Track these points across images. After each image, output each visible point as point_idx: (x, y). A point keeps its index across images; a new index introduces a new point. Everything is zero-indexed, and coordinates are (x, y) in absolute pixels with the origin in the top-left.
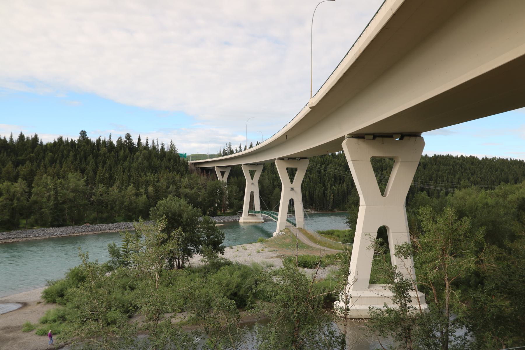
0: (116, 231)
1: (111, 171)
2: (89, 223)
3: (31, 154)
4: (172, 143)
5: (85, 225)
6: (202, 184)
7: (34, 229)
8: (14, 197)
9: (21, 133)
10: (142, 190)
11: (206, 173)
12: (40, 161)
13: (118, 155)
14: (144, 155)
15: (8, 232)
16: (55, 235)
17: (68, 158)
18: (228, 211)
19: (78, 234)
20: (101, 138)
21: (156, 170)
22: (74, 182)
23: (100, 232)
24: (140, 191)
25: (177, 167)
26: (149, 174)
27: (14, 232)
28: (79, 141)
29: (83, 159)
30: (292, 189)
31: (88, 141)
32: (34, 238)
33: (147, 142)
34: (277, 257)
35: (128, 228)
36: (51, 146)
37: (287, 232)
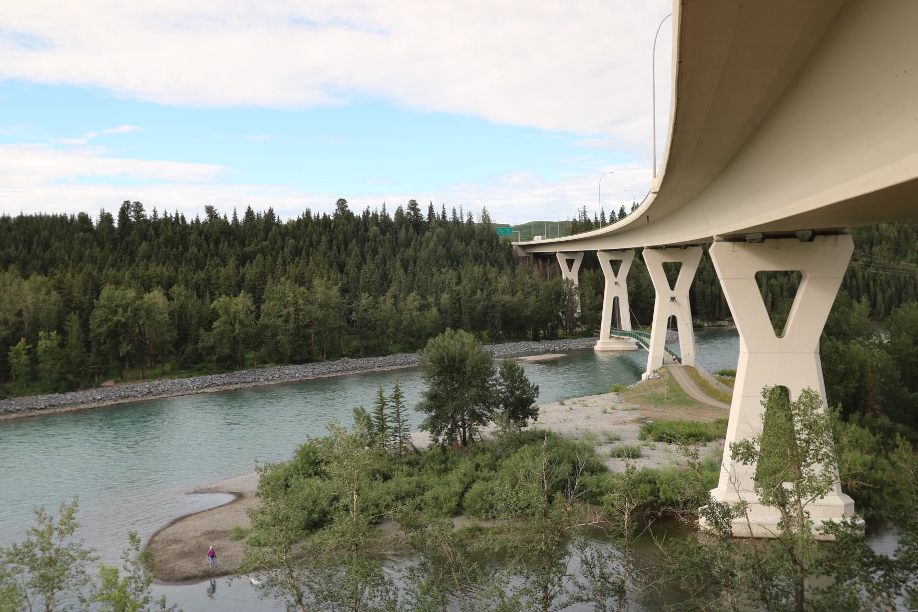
0: (389, 368)
1: (385, 266)
2: (348, 356)
3: (264, 243)
4: (485, 213)
5: (342, 359)
6: (532, 285)
7: (266, 367)
8: (235, 320)
9: (249, 208)
10: (431, 300)
11: (543, 264)
12: (278, 253)
13: (396, 238)
14: (438, 236)
15: (230, 374)
16: (296, 378)
17: (318, 247)
18: (578, 330)
19: (330, 376)
20: (369, 209)
21: (458, 262)
22: (323, 292)
23: (365, 371)
24: (429, 300)
25: (492, 254)
26: (446, 269)
27: (237, 373)
28: (336, 215)
29: (342, 248)
30: (673, 299)
31: (349, 216)
32: (266, 383)
33: (444, 213)
34: (634, 421)
35: (409, 363)
36: (293, 227)
37: (664, 374)
